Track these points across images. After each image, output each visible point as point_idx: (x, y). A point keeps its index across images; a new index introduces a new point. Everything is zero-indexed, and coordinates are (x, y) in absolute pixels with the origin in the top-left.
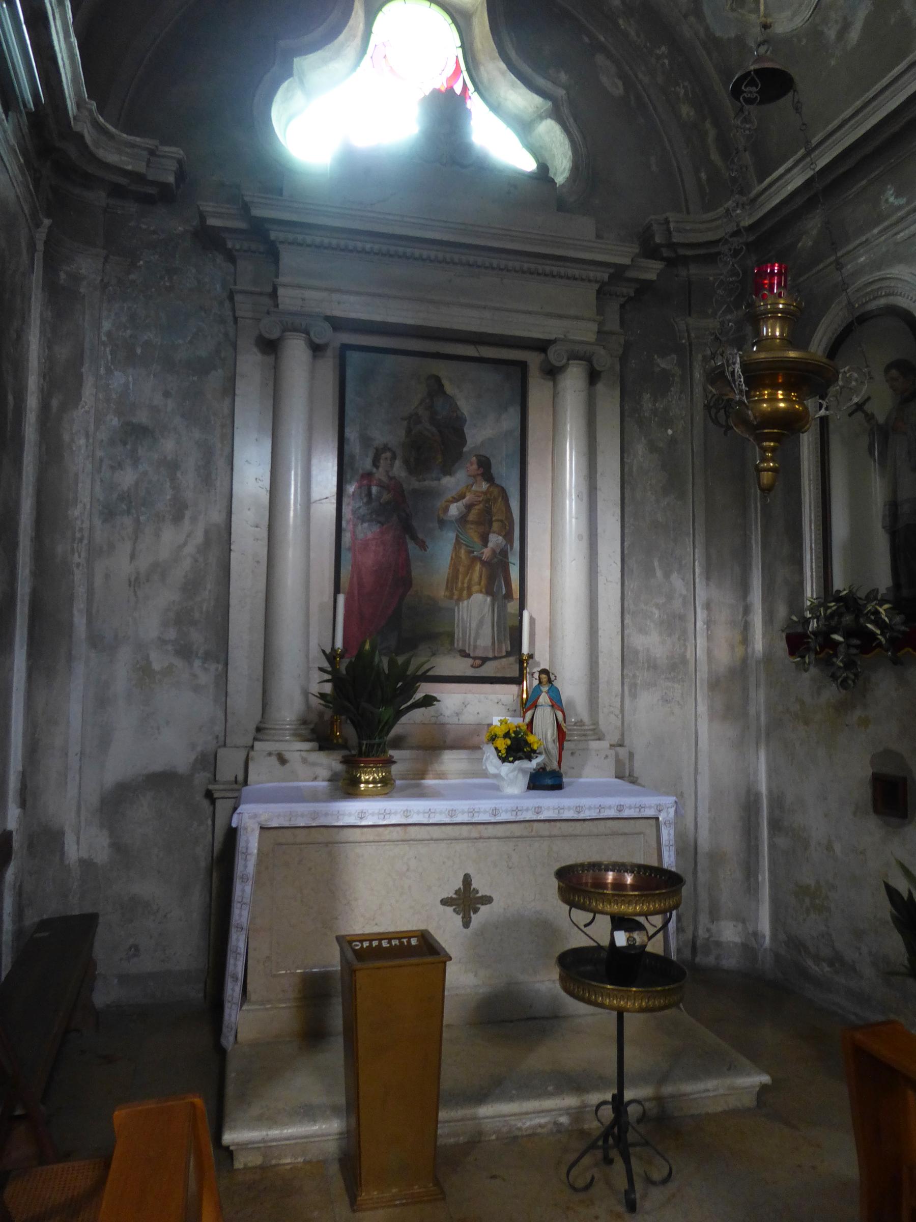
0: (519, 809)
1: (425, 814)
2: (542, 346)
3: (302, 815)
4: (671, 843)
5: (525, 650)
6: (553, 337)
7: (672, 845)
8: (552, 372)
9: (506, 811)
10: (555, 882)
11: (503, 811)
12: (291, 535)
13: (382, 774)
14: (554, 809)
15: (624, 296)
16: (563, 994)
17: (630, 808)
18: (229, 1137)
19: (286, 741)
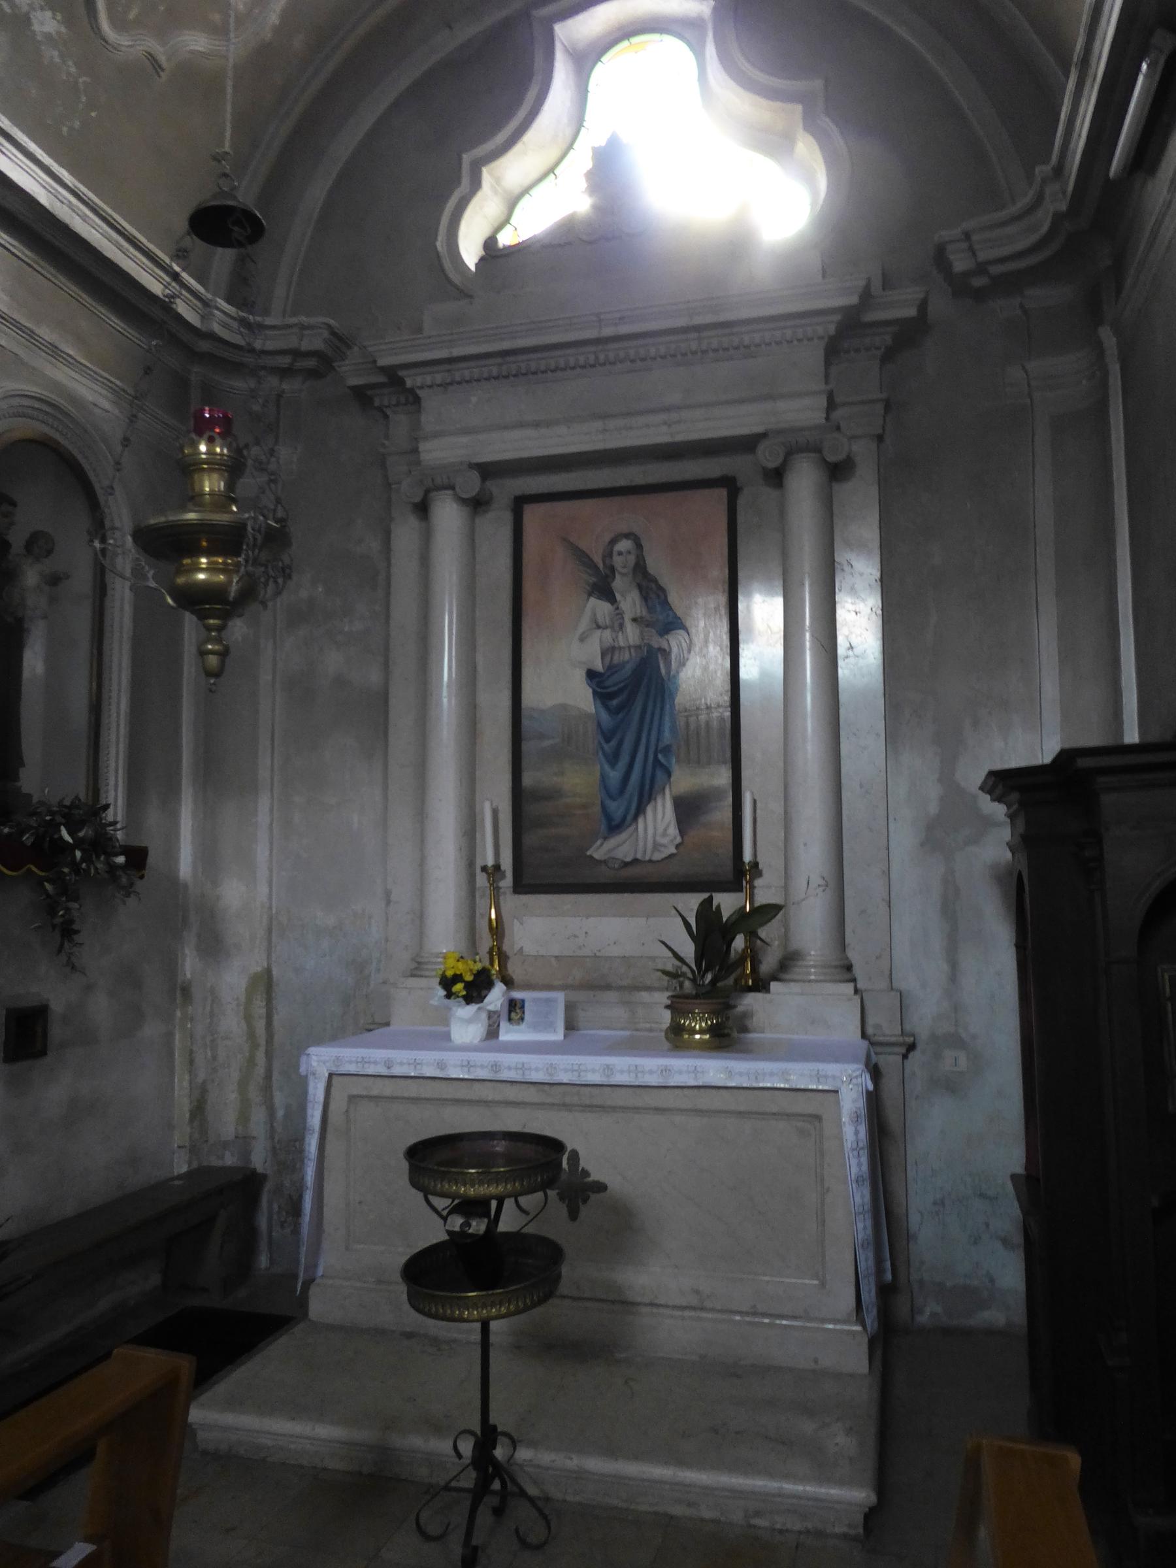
0: (417, 1061)
1: (575, 1073)
2: (747, 444)
3: (651, 1072)
4: (861, 1145)
5: (747, 857)
6: (759, 429)
7: (862, 1148)
8: (776, 477)
9: (566, 1071)
10: (405, 1165)
11: (487, 1067)
12: (445, 718)
13: (685, 1022)
14: (516, 1069)
15: (878, 348)
16: (421, 1318)
17: (509, 1068)
18: (861, 1496)
19: (810, 981)
